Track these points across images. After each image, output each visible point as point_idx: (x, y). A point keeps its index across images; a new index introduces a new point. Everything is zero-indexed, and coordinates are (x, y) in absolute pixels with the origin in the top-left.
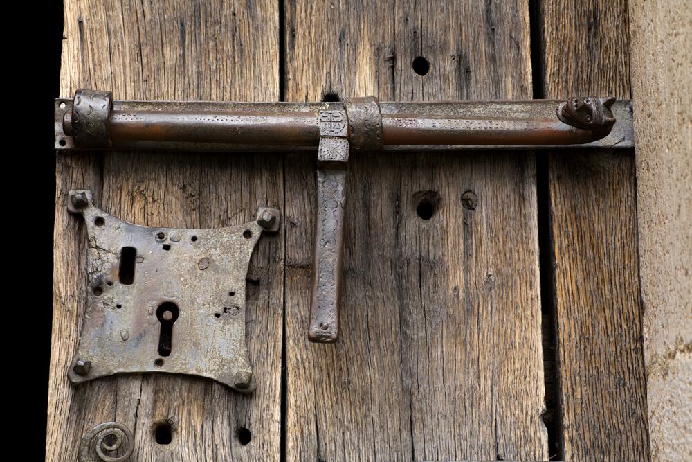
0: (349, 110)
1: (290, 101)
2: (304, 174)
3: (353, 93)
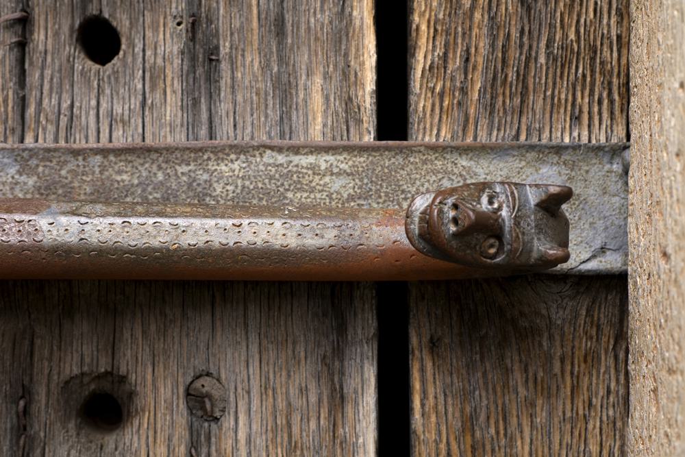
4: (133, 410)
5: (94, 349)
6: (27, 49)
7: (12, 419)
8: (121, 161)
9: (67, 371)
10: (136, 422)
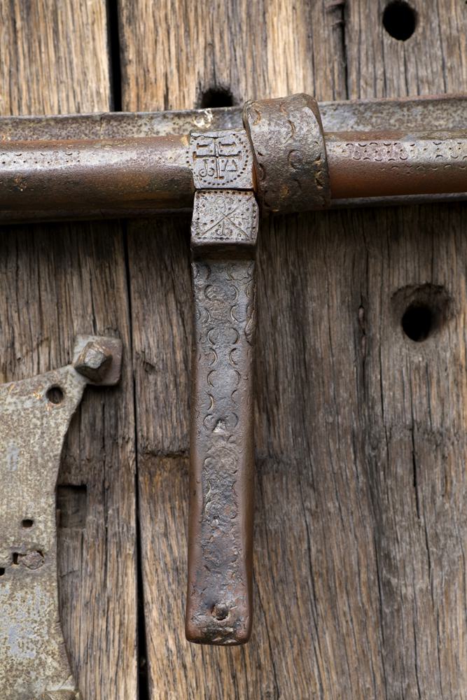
0: (255, 129)
2: (168, 263)
3: (262, 85)
4: (448, 314)
5: (416, 265)
6: (346, 30)
7: (354, 324)
8: (438, 110)
9: (396, 285)
10: (452, 324)
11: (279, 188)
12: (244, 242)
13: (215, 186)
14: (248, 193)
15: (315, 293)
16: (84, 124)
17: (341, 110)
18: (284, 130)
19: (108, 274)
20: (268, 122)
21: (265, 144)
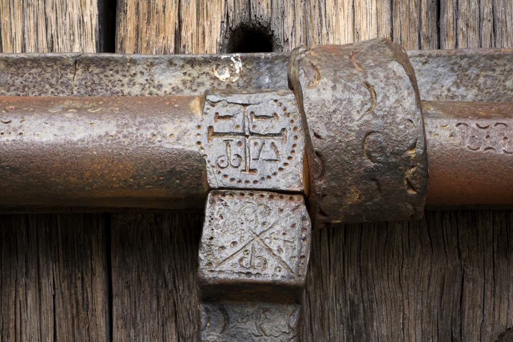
0: (311, 95)
1: (129, 53)
2: (169, 277)
3: (316, 21)
9: (503, 321)
11: (345, 192)
12: (286, 281)
13: (242, 185)
14: (296, 197)
15: (384, 331)
16: (49, 70)
17: (432, 65)
18: (357, 99)
19: (79, 289)
20: (331, 84)
21: (326, 120)
